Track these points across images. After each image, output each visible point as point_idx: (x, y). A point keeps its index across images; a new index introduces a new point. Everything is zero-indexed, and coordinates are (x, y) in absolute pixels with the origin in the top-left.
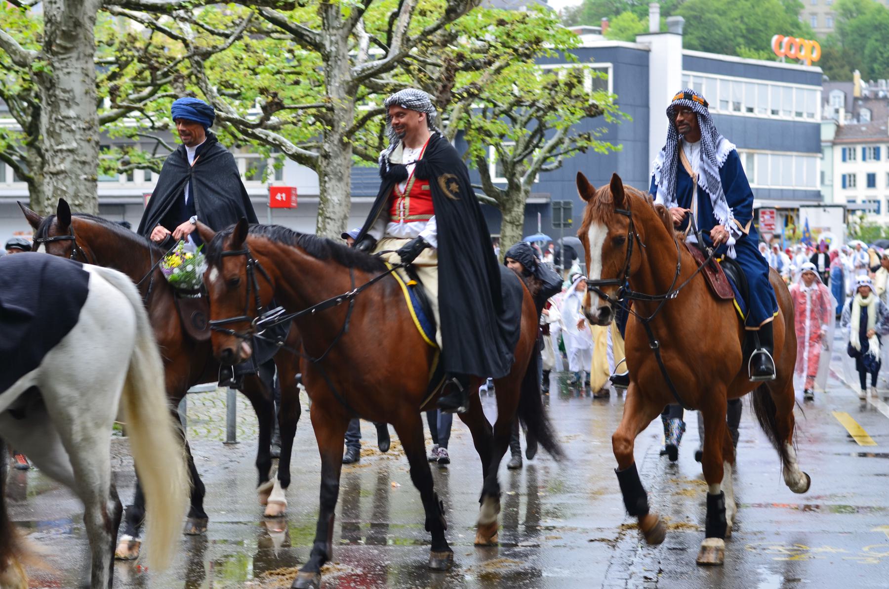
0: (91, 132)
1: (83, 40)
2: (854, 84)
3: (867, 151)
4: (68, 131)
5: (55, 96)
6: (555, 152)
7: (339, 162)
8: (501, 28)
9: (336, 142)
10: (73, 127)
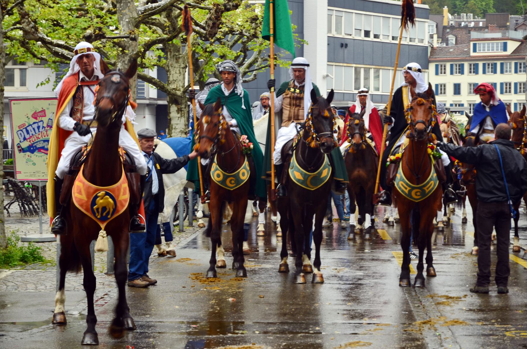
2: (444, 17)
3: (454, 67)
6: (251, 69)
9: (126, 62)
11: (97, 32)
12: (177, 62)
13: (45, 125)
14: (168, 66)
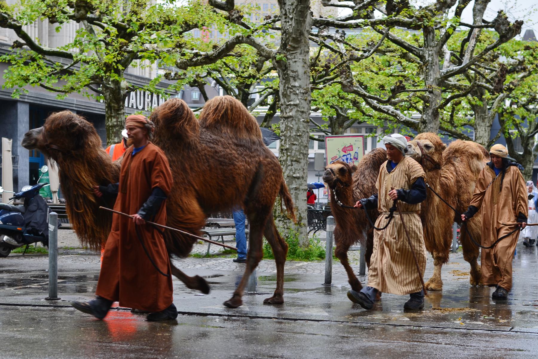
0: (307, 95)
1: (304, 43)
4: (294, 94)
5: (288, 74)
7: (432, 126)
8: (528, 51)
9: (430, 114)
10: (297, 92)
11: (398, 84)
12: (483, 121)
13: (352, 157)
14: (476, 125)
